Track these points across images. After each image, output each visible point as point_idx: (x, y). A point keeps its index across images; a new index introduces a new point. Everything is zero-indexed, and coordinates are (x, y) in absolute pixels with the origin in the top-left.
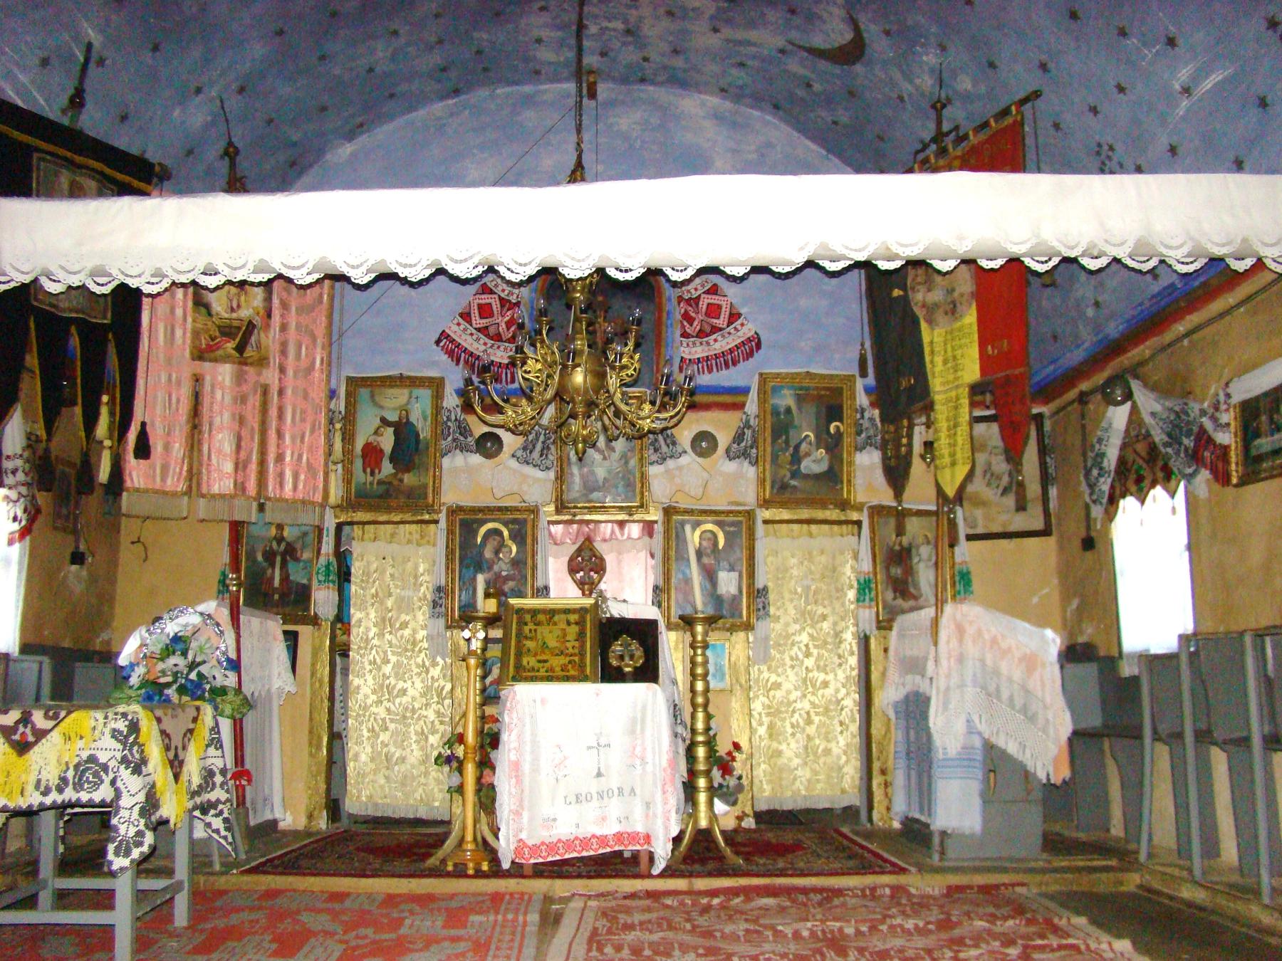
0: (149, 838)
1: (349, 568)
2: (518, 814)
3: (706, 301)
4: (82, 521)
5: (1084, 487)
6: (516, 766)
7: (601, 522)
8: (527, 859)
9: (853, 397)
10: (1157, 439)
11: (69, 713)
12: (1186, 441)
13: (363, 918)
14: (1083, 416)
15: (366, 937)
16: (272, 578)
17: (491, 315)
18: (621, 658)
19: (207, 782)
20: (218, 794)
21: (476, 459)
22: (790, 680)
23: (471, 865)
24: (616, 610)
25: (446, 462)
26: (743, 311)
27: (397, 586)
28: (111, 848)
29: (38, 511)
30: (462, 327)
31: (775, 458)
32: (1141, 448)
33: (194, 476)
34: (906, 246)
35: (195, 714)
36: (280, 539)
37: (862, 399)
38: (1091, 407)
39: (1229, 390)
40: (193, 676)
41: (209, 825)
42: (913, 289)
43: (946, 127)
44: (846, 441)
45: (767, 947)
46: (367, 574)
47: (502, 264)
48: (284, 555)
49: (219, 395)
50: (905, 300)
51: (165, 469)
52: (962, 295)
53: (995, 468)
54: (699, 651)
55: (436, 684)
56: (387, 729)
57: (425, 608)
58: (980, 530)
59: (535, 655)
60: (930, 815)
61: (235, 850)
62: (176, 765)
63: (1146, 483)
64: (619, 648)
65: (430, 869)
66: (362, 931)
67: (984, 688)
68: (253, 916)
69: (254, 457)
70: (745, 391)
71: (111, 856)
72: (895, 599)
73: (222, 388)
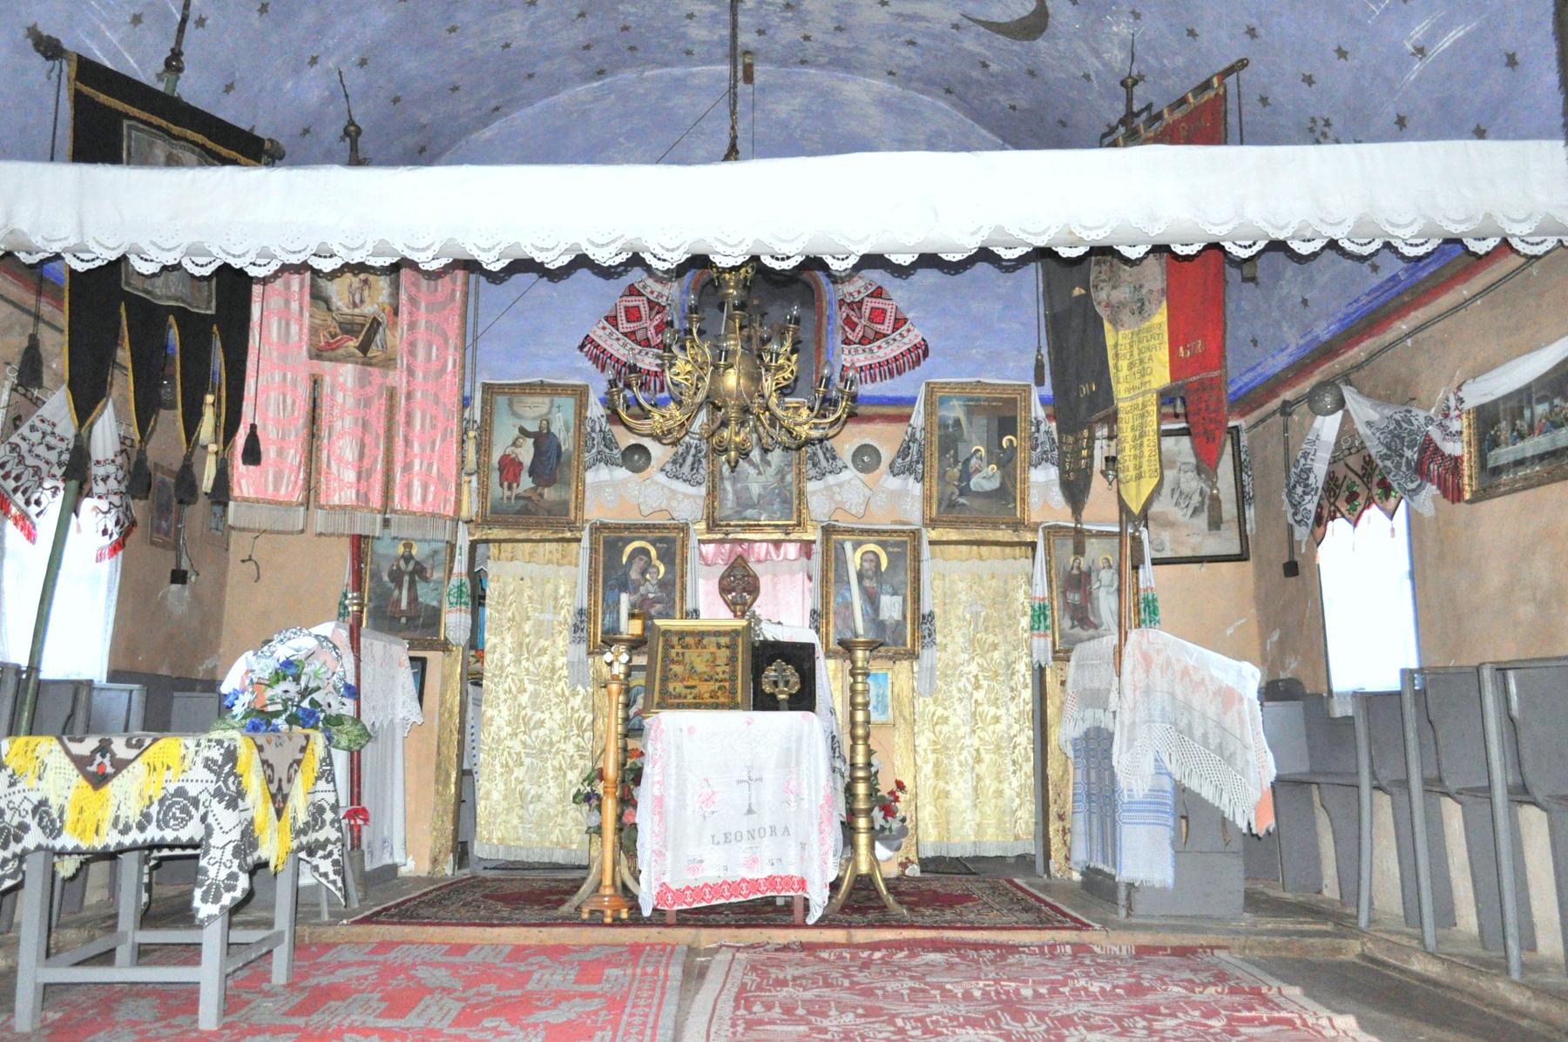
0: (243, 882)
2: (660, 854)
3: (870, 305)
4: (185, 534)
5: (1287, 507)
6: (660, 801)
7: (756, 541)
9: (1028, 409)
10: (1373, 452)
11: (155, 740)
12: (1408, 453)
13: (486, 973)
14: (1286, 429)
16: (399, 601)
17: (639, 319)
18: (776, 683)
19: (315, 820)
21: (622, 473)
22: (958, 713)
23: (609, 912)
24: (770, 633)
25: (590, 476)
26: (909, 316)
27: (535, 610)
28: (198, 893)
29: (133, 524)
30: (608, 331)
31: (942, 475)
32: (1355, 462)
33: (310, 488)
34: (1091, 229)
35: (304, 743)
36: (408, 558)
37: (1038, 411)
38: (1295, 417)
39: (1461, 394)
40: (305, 704)
41: (316, 868)
44: (1020, 455)
45: (934, 1008)
46: (502, 595)
47: (647, 250)
48: (412, 574)
49: (340, 397)
50: (1087, 300)
51: (278, 478)
52: (1151, 291)
54: (860, 679)
55: (576, 715)
56: (522, 764)
57: (565, 633)
58: (1167, 554)
59: (681, 681)
60: (1114, 865)
61: (346, 897)
62: (279, 800)
63: (1361, 500)
64: (773, 673)
66: (484, 988)
67: (1175, 724)
68: (364, 971)
69: (379, 466)
70: (911, 402)
71: (197, 903)
72: (1073, 627)
73: (344, 390)
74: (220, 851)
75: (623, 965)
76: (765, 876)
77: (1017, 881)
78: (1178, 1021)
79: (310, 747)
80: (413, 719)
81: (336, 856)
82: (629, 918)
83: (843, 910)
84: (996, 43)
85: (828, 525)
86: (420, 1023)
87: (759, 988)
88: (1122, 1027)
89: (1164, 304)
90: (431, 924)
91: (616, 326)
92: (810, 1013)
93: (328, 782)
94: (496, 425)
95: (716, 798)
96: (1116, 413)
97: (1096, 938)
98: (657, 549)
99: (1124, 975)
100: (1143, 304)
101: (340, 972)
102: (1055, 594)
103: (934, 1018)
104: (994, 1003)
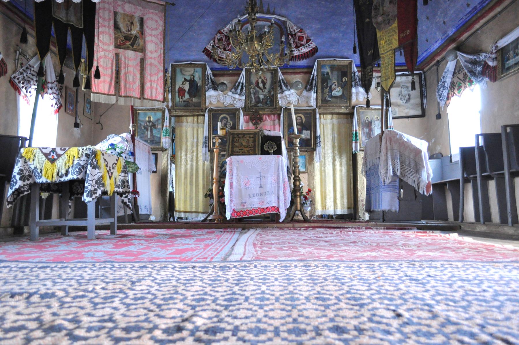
25: (208, 94)
26: (312, 38)
36: (150, 121)
37: (354, 69)
39: (497, 44)
48: (151, 127)
50: (370, 22)
58: (397, 115)
81: (129, 197)
89: (397, 20)
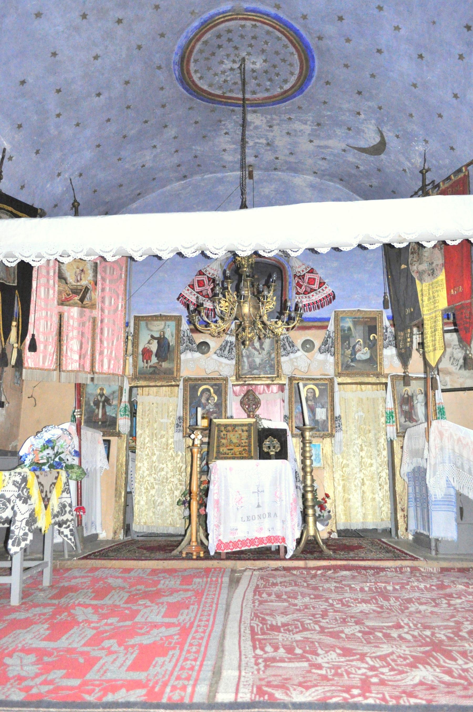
1: (136, 410)
2: (218, 526)
3: (308, 277)
6: (217, 502)
7: (258, 385)
8: (223, 550)
13: (140, 581)
15: (139, 590)
16: (98, 414)
18: (269, 447)
19: (62, 510)
20: (67, 516)
22: (354, 462)
23: (195, 553)
24: (266, 424)
25: (183, 356)
26: (326, 281)
30: (190, 291)
35: (57, 475)
36: (102, 395)
37: (387, 323)
40: (57, 459)
42: (411, 264)
43: (427, 182)
44: (379, 343)
45: (347, 595)
47: (208, 250)
49: (71, 322)
50: (408, 269)
52: (437, 265)
53: (455, 356)
54: (308, 445)
55: (178, 466)
56: (154, 488)
57: (173, 428)
58: (449, 387)
61: (76, 546)
62: (46, 501)
64: (268, 443)
65: (175, 556)
66: (139, 587)
67: (455, 464)
68: (84, 580)
69: (89, 352)
70: (328, 320)
72: (406, 421)
74: (20, 523)
75: (202, 577)
76: (266, 536)
77: (383, 540)
78: (462, 600)
79: (59, 477)
80: (105, 467)
81: (71, 527)
82: (204, 556)
83: (302, 552)
84: (362, 158)
85: (292, 377)
86: (110, 602)
87: (265, 587)
88: (436, 603)
89: (444, 271)
90: (115, 559)
91: (193, 289)
92: (289, 597)
93: (67, 493)
94: (141, 336)
95: (243, 500)
96: (423, 320)
97: (422, 564)
98: (214, 389)
99: (435, 580)
100: (434, 271)
101: (73, 581)
102: (397, 406)
103: (347, 599)
104: (374, 592)
